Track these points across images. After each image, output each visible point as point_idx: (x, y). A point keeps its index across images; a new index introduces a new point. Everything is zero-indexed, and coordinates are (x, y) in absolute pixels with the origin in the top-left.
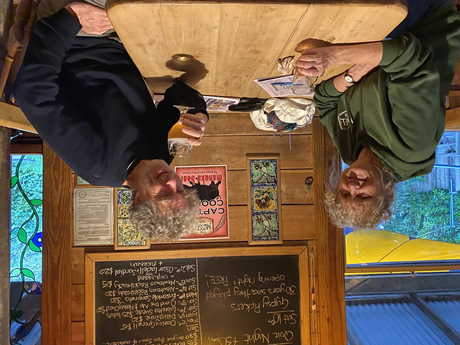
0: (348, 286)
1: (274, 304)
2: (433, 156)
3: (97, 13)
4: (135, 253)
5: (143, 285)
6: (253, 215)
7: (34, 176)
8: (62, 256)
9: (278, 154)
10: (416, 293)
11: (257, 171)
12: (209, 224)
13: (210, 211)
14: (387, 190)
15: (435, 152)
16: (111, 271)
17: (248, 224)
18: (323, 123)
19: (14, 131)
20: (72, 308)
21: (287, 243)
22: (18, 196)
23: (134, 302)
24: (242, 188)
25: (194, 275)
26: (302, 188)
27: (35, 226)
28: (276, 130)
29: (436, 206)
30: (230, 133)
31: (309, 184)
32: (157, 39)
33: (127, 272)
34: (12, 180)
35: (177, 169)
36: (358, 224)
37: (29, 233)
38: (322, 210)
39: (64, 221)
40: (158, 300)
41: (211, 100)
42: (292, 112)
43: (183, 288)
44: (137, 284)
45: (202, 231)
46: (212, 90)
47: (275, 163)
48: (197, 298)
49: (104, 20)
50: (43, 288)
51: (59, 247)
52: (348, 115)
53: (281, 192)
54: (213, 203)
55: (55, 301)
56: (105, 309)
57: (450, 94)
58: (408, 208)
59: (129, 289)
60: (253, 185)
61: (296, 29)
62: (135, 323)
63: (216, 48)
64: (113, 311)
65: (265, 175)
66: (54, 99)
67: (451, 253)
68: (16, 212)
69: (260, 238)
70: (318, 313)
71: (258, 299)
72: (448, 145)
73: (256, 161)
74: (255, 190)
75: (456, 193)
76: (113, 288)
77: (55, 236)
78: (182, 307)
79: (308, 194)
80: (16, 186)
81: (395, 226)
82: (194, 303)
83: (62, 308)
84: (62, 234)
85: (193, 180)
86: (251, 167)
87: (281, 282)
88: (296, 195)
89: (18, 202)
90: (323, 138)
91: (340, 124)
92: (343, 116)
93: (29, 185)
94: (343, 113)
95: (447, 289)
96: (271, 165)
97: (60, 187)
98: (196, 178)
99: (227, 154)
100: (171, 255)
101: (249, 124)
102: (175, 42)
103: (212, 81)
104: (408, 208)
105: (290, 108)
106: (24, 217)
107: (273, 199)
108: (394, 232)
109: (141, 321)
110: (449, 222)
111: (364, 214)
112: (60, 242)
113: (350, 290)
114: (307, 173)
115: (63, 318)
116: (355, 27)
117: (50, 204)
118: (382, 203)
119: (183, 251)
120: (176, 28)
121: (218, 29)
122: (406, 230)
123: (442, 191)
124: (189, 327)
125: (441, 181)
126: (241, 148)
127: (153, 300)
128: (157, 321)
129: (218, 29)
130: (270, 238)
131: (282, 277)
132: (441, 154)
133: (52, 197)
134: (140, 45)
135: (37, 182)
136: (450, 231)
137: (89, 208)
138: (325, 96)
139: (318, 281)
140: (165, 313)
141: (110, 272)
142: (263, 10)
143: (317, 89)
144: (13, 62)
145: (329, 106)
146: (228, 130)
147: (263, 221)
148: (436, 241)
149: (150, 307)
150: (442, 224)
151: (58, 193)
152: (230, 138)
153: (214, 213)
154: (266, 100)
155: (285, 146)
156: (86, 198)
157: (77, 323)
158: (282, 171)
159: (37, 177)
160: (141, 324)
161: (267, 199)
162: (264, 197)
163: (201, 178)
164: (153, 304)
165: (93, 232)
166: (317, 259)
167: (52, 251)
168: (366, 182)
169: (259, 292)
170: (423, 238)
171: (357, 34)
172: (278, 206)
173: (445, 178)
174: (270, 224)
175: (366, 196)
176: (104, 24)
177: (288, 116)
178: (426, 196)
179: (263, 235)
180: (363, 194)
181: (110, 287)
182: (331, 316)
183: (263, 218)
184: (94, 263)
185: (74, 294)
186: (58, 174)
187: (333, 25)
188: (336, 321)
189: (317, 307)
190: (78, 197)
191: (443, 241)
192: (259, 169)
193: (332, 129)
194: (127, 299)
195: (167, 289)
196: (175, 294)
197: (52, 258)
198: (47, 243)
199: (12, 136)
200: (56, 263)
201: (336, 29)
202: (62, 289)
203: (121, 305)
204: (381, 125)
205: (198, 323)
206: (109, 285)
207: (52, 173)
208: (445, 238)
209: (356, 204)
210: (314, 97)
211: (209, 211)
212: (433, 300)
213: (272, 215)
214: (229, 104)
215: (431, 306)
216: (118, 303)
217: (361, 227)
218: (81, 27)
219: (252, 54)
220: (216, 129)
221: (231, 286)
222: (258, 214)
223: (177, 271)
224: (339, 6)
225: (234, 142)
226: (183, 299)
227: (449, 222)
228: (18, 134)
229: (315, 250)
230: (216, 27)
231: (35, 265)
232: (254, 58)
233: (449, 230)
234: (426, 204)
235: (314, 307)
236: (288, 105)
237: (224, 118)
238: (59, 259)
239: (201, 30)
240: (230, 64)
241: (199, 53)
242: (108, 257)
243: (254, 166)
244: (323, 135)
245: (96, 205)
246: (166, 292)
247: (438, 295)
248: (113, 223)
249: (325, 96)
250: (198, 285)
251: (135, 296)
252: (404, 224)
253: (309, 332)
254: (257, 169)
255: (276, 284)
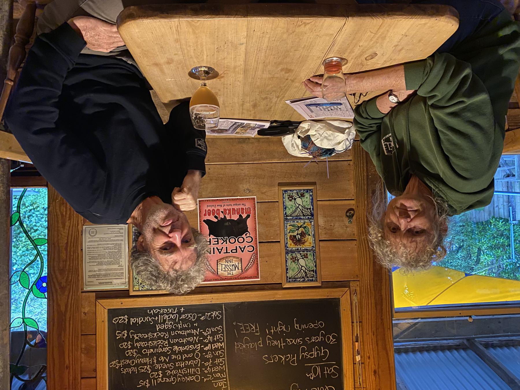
1: (312, 355)
2: (491, 185)
3: (103, 28)
4: (153, 299)
5: (162, 334)
6: (287, 253)
7: (38, 209)
9: (314, 184)
10: (474, 338)
11: (291, 203)
17: (281, 264)
18: (365, 149)
19: (14, 163)
20: (81, 363)
21: (327, 285)
22: (21, 232)
23: (152, 355)
24: (274, 222)
25: (220, 322)
26: (343, 221)
27: (40, 266)
28: (311, 157)
29: (494, 238)
30: (259, 160)
31: (350, 217)
32: (176, 58)
33: (144, 320)
34: (13, 216)
35: (200, 201)
36: (409, 263)
37: (33, 274)
38: (366, 247)
39: (71, 262)
42: (330, 136)
43: (208, 338)
44: (155, 334)
45: (229, 272)
46: (239, 114)
47: (311, 193)
48: (224, 349)
49: (111, 37)
50: (48, 340)
51: (66, 293)
52: (393, 138)
53: (318, 226)
54: (241, 240)
55: (62, 354)
56: (119, 363)
57: (508, 114)
58: (463, 241)
59: (147, 340)
60: (286, 219)
61: (333, 44)
62: (154, 379)
63: (242, 67)
64: (129, 366)
65: (300, 207)
67: (513, 291)
68: (18, 250)
70: (363, 365)
71: (293, 349)
72: (506, 168)
73: (289, 192)
74: (288, 225)
75: (516, 222)
76: (128, 339)
77: (61, 281)
78: (207, 360)
79: (350, 228)
80: (18, 223)
81: (448, 261)
82: (221, 355)
83: (71, 363)
85: (219, 214)
86: (284, 198)
87: (320, 329)
89: (21, 239)
90: (365, 165)
91: (384, 149)
92: (388, 140)
93: (33, 219)
95: (509, 334)
96: (307, 195)
97: (67, 224)
98: (222, 212)
99: (257, 183)
100: (195, 300)
103: (238, 103)
104: (463, 241)
105: (327, 132)
106: (27, 257)
107: (309, 235)
108: (447, 267)
110: (509, 256)
111: (417, 251)
112: (68, 287)
113: (397, 336)
117: (56, 244)
118: (436, 239)
122: (461, 265)
123: (501, 221)
124: (216, 383)
125: (499, 209)
126: (272, 177)
127: (174, 353)
130: (306, 279)
131: (321, 324)
132: (498, 179)
133: (58, 236)
134: (156, 65)
135: (42, 216)
138: (367, 118)
139: (362, 328)
140: (187, 367)
143: (357, 110)
144: (12, 86)
145: (371, 129)
146: (257, 156)
147: (298, 260)
148: (496, 277)
149: (170, 360)
150: (501, 258)
153: (243, 251)
154: (300, 123)
155: (322, 174)
156: (97, 236)
158: (318, 202)
159: (42, 211)
161: (303, 234)
163: (227, 212)
164: (174, 357)
165: (105, 275)
166: (360, 303)
167: (59, 296)
169: (295, 342)
172: (315, 243)
173: (504, 205)
174: (307, 263)
175: (418, 230)
176: (112, 41)
177: (325, 140)
178: (483, 226)
179: (299, 275)
181: (125, 337)
182: (378, 368)
183: (299, 256)
184: (106, 311)
185: (83, 346)
186: (64, 209)
187: (374, 39)
188: (384, 372)
189: (361, 357)
190: (87, 235)
191: (503, 277)
192: (293, 200)
194: (145, 351)
195: (191, 339)
197: (59, 305)
200: (63, 312)
201: (378, 44)
204: (431, 150)
205: (226, 378)
206: (124, 335)
208: (505, 273)
209: (408, 241)
211: (236, 249)
212: (494, 346)
213: (309, 253)
214: (258, 128)
215: (492, 353)
218: (85, 43)
219: (283, 73)
220: (243, 155)
221: (264, 335)
222: (292, 252)
223: (199, 318)
225: (263, 170)
226: (208, 350)
227: (509, 256)
228: (19, 165)
229: (358, 292)
230: (243, 44)
231: (40, 310)
232: (286, 78)
234: (482, 235)
235: (358, 358)
237: (252, 143)
239: (226, 47)
240: (258, 84)
242: (122, 303)
243: (287, 197)
245: (108, 244)
246: (189, 343)
247: (499, 341)
249: (367, 118)
250: (225, 335)
253: (353, 387)
254: (291, 200)
255: (315, 332)
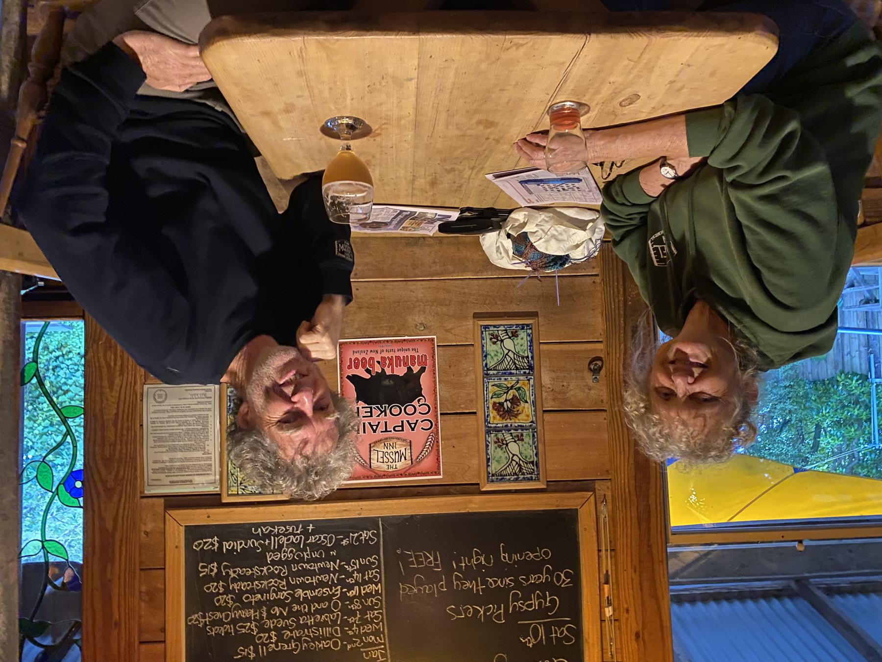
0: (674, 565)
1: (530, 606)
2: (833, 318)
4: (262, 509)
5: (276, 569)
6: (488, 432)
7: (70, 355)
8: (121, 515)
9: (534, 315)
10: (807, 578)
11: (494, 347)
12: (403, 450)
13: (406, 425)
14: (747, 384)
15: (836, 309)
16: (216, 543)
17: (478, 451)
19: (28, 280)
20: (140, 617)
23: (260, 604)
24: (467, 379)
25: (375, 550)
26: (583, 378)
28: (529, 269)
29: (843, 407)
30: (442, 274)
31: (596, 371)
34: (27, 368)
37: (62, 465)
40: (306, 599)
41: (405, 213)
42: (561, 234)
44: (265, 569)
46: (407, 196)
47: (529, 331)
48: (381, 595)
50: (85, 576)
51: (116, 498)
54: (410, 410)
55: (107, 601)
56: (204, 617)
57: (864, 197)
58: (790, 411)
59: (251, 578)
60: (487, 374)
61: (566, 76)
62: (263, 644)
63: (412, 117)
65: (510, 354)
66: (102, 219)
68: (36, 425)
69: (501, 477)
70: (617, 623)
71: (498, 596)
72: (863, 288)
73: (492, 328)
76: (219, 577)
77: (106, 476)
78: (353, 613)
79: (594, 391)
80: (34, 381)
82: (377, 604)
83: (123, 617)
84: (122, 473)
85: (373, 366)
86: (483, 339)
88: (572, 393)
89: (40, 406)
90: (621, 283)
92: (658, 241)
93: (61, 373)
94: (658, 234)
96: (522, 334)
97: (117, 381)
98: (378, 362)
99: (437, 314)
100: (332, 512)
101: (477, 256)
102: (333, 108)
103: (405, 178)
104: (790, 411)
106: (50, 438)
107: (526, 402)
108: (764, 457)
109: (273, 641)
110: (869, 438)
113: (676, 574)
114: (591, 350)
115: (123, 635)
116: (677, 75)
118: (737, 410)
119: (353, 503)
120: (335, 82)
121: (414, 82)
122: (786, 454)
123: (855, 378)
125: (852, 357)
126: (463, 302)
127: (296, 600)
128: (306, 641)
129: (414, 82)
130: (521, 477)
131: (546, 553)
132: (851, 307)
133: (102, 402)
134: (266, 114)
135: (76, 368)
136: (873, 456)
137: (173, 422)
138: (623, 204)
140: (319, 625)
141: (214, 545)
142: (500, 46)
143: (607, 190)
144: (25, 150)
147: (507, 445)
149: (290, 612)
151: (114, 393)
152: (441, 284)
153: (413, 429)
155: (548, 298)
157: (150, 646)
159: (76, 359)
160: (273, 646)
161: (515, 401)
162: (510, 397)
163: (387, 362)
164: (296, 607)
165: (181, 469)
166: (613, 518)
167: (102, 505)
168: (706, 368)
170: (820, 469)
171: (682, 88)
172: (536, 415)
173: (860, 352)
174: (522, 450)
177: (553, 241)
178: (824, 387)
179: (509, 470)
180: (702, 393)
181: (213, 574)
182: (643, 629)
183: (508, 437)
184: (182, 529)
185: (144, 589)
187: (635, 72)
189: (614, 610)
191: (857, 474)
192: (499, 343)
193: (637, 265)
194: (247, 598)
195: (324, 578)
196: (339, 587)
197: (102, 519)
198: (93, 491)
199: (24, 289)
202: (122, 581)
203: (234, 609)
205: (384, 644)
206: (212, 571)
207: (101, 354)
208: (863, 468)
209: (689, 414)
210: (603, 205)
211: (402, 426)
213: (525, 433)
214: (439, 220)
215: (837, 603)
216: (229, 606)
217: (698, 457)
219: (481, 127)
220: (414, 266)
221: (448, 571)
222: (497, 430)
223: (340, 542)
224: (645, 37)
225: (449, 292)
226: (355, 597)
227: (869, 438)
228: (36, 283)
229: (609, 499)
230: (411, 79)
233: (871, 453)
235: (608, 611)
236: (552, 221)
237: (430, 245)
238: (115, 520)
239: (384, 84)
240: (439, 146)
241: (380, 128)
242: (209, 517)
243: (488, 337)
244: (621, 276)
246: (322, 584)
247: (851, 583)
248: (218, 450)
249: (623, 204)
251: (262, 592)
252: (783, 443)
254: (494, 343)
255: (535, 567)
